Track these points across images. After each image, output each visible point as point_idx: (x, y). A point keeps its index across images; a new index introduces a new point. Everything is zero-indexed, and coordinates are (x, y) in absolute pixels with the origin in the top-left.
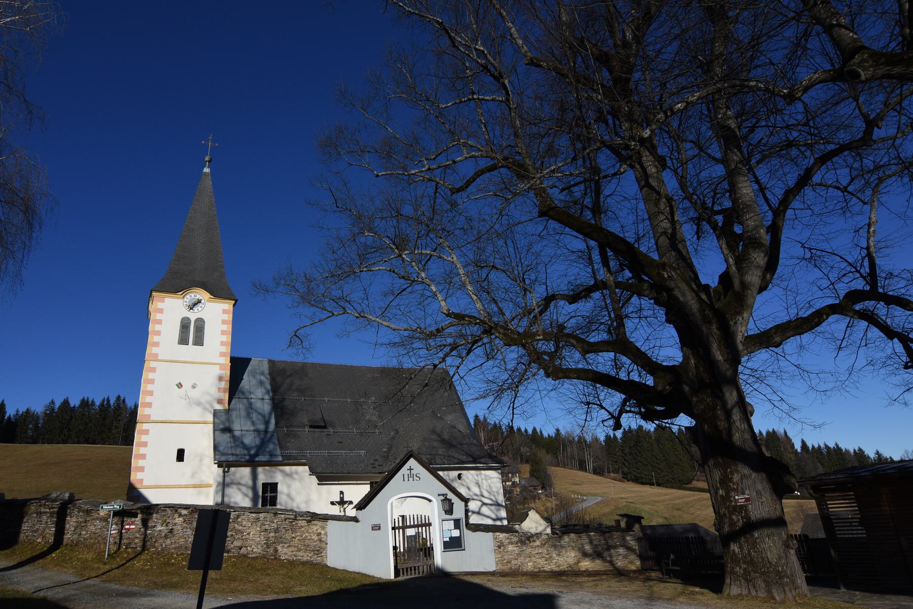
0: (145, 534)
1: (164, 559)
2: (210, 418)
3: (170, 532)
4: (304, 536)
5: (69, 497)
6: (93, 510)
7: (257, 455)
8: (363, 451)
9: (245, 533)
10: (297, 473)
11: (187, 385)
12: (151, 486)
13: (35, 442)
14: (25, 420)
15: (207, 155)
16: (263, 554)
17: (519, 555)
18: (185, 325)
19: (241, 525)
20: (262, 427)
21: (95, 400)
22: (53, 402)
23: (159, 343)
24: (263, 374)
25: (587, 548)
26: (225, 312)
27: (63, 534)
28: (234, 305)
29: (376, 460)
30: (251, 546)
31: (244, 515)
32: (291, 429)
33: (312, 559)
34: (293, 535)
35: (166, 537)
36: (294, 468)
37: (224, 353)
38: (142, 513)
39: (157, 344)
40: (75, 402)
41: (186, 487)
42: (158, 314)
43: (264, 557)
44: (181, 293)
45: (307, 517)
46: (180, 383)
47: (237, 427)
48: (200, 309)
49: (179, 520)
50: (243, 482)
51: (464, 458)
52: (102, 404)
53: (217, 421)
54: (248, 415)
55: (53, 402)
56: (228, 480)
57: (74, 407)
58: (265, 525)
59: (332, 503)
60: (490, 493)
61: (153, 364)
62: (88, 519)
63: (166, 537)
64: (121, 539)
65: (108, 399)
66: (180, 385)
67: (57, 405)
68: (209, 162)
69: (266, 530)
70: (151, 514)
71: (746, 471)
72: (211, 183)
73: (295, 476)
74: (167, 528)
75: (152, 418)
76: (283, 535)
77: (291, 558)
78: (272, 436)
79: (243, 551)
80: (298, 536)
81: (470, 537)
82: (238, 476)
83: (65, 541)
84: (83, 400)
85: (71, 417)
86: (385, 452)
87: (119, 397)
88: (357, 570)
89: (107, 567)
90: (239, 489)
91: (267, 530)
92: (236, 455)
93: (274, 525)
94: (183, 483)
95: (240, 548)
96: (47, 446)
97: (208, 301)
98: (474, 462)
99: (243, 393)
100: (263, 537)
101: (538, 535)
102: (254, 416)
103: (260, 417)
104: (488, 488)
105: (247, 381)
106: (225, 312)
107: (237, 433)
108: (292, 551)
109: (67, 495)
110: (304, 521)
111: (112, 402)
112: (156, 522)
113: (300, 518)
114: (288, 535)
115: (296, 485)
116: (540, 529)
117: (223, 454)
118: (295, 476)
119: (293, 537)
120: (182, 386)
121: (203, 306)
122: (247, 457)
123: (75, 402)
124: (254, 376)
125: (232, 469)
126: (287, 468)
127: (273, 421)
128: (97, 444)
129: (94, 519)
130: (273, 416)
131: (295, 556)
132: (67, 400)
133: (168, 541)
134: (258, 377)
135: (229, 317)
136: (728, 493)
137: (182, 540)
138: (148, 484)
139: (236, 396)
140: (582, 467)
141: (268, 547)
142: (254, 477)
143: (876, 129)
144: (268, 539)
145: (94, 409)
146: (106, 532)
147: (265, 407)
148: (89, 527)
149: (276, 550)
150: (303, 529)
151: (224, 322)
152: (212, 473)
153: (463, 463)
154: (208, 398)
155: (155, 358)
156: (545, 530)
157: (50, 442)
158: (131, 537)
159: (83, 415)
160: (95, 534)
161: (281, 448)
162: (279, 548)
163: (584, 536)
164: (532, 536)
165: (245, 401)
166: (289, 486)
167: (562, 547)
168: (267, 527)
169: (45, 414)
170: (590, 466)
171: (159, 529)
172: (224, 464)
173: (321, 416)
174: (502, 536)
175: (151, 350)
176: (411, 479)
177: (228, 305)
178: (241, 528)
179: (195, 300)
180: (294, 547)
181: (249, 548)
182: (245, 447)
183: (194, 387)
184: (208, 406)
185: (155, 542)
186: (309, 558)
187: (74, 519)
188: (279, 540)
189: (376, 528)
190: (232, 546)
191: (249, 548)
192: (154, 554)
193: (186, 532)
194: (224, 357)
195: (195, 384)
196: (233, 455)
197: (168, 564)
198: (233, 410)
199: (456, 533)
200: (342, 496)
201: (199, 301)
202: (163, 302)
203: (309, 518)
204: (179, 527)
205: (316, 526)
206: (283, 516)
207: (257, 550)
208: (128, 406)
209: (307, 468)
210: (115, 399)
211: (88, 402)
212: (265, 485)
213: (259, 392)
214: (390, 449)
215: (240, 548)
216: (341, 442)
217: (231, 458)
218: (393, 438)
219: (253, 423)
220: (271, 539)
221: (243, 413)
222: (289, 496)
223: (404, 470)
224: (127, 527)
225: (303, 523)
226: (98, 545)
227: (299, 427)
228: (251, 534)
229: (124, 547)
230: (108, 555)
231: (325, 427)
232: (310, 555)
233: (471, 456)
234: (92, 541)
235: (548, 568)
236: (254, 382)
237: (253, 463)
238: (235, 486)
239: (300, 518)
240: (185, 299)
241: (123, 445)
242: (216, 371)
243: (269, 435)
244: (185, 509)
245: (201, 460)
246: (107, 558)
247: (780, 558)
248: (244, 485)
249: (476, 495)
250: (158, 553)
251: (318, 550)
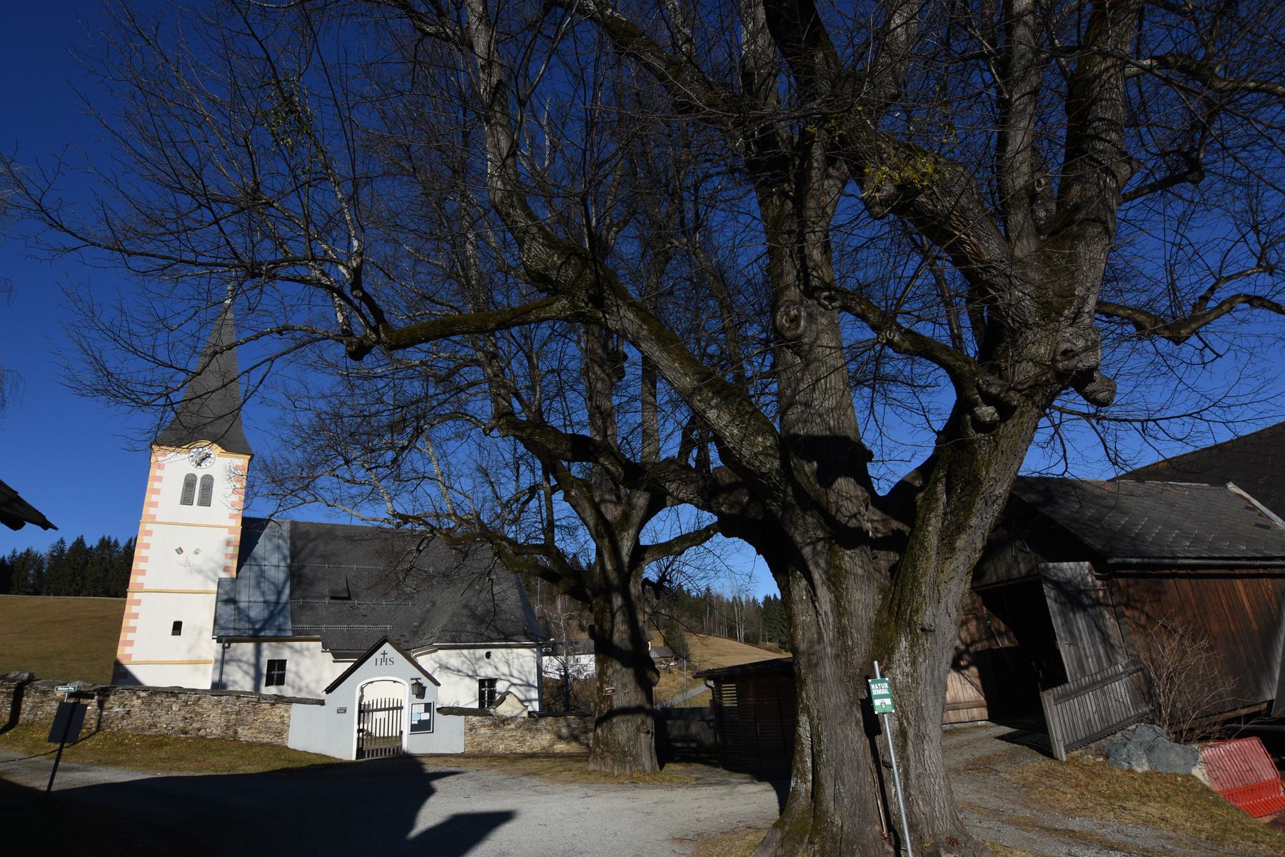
0: (100, 715)
2: (214, 588)
7: (261, 629)
10: (308, 649)
13: (37, 593)
14: (24, 563)
17: (491, 737)
18: (189, 483)
20: (272, 598)
22: (62, 542)
24: (281, 537)
25: (564, 731)
27: (19, 714)
32: (309, 600)
35: (123, 718)
36: (305, 644)
38: (98, 694)
39: (155, 504)
40: (92, 542)
47: (244, 598)
48: (208, 464)
49: (137, 702)
50: (244, 659)
51: (494, 635)
53: (220, 591)
54: (258, 585)
55: (62, 542)
56: (227, 657)
57: (91, 548)
60: (520, 672)
61: (148, 527)
63: (123, 718)
67: (68, 545)
69: (227, 713)
70: (108, 696)
71: (618, 666)
73: (306, 653)
75: (146, 587)
78: (284, 608)
79: (202, 732)
81: (440, 720)
82: (239, 652)
83: (20, 721)
84: (103, 539)
85: (87, 561)
86: (415, 627)
88: (318, 751)
90: (240, 667)
92: (239, 630)
93: (237, 708)
94: (178, 659)
96: (52, 598)
97: (219, 456)
98: (506, 639)
99: (255, 559)
101: (513, 719)
102: (265, 586)
103: (272, 587)
104: (519, 668)
105: (263, 546)
107: (242, 605)
109: (26, 675)
114: (250, 718)
115: (306, 663)
116: (516, 712)
117: (223, 628)
118: (306, 653)
122: (251, 632)
123: (92, 542)
124: (270, 540)
125: (233, 645)
126: (297, 644)
127: (287, 591)
130: (288, 585)
132: (82, 539)
133: (125, 722)
134: (276, 540)
136: (601, 685)
139: (248, 562)
140: (732, 635)
141: (228, 728)
142: (258, 653)
144: (228, 721)
147: (279, 575)
149: (236, 732)
152: (211, 649)
153: (492, 640)
154: (213, 565)
155: (152, 519)
156: (521, 713)
157: (57, 593)
159: (103, 559)
161: (293, 622)
162: (240, 730)
163: (561, 720)
164: (507, 719)
165: (256, 568)
166: (297, 664)
167: (538, 730)
168: (228, 709)
169: (52, 556)
170: (741, 633)
173: (345, 586)
174: (474, 719)
175: (148, 511)
176: (384, 663)
177: (241, 461)
179: (203, 455)
182: (250, 620)
183: (196, 553)
184: (211, 574)
187: (30, 700)
188: (240, 722)
189: (342, 711)
196: (235, 629)
197: (121, 744)
198: (241, 578)
199: (426, 716)
201: (208, 456)
204: (137, 709)
205: (280, 709)
207: (217, 732)
209: (320, 643)
211: (109, 542)
212: (271, 663)
213: (275, 558)
214: (421, 623)
215: (199, 730)
217: (232, 633)
218: (428, 611)
219: (263, 594)
221: (253, 582)
222: (297, 674)
223: (378, 655)
225: (267, 706)
227: (316, 598)
231: (349, 598)
233: (503, 633)
235: (519, 750)
236: (269, 546)
237: (256, 638)
238: (234, 663)
242: (224, 535)
245: (200, 634)
247: (629, 739)
248: (247, 663)
249: (504, 675)
250: (113, 734)
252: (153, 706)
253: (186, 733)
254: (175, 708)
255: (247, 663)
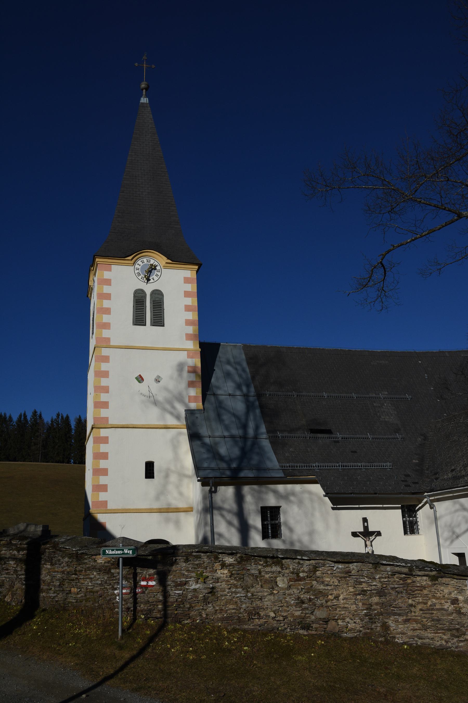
1: (211, 639)
3: (210, 593)
4: (429, 603)
5: (43, 531)
6: (86, 554)
8: (388, 464)
9: (330, 597)
10: (293, 494)
11: (149, 378)
12: (129, 509)
15: (143, 81)
16: (366, 634)
19: (323, 582)
20: (236, 432)
21: (12, 416)
26: (187, 280)
28: (197, 272)
29: (408, 476)
30: (343, 619)
31: (324, 565)
33: (450, 644)
34: (410, 601)
36: (289, 486)
41: (150, 511)
43: (367, 637)
44: (130, 258)
45: (431, 571)
46: (140, 375)
48: (156, 278)
49: (223, 573)
52: (19, 420)
58: (361, 583)
59: (355, 534)
62: (79, 568)
63: (205, 600)
64: (135, 602)
65: (25, 414)
66: (140, 379)
68: (147, 89)
69: (363, 592)
72: (151, 116)
73: (292, 498)
74: (206, 586)
75: (111, 422)
76: (395, 600)
77: (411, 641)
80: (419, 603)
87: (35, 412)
89: (127, 655)
91: (365, 591)
95: (326, 621)
97: (165, 267)
100: (360, 604)
102: (226, 417)
106: (187, 280)
108: (414, 630)
110: (425, 578)
111: (29, 418)
112: (187, 577)
113: (420, 573)
118: (292, 498)
119: (411, 605)
121: (159, 274)
122: (228, 473)
126: (281, 488)
128: (17, 461)
129: (89, 569)
131: (420, 638)
133: (210, 608)
135: (192, 287)
137: (231, 607)
138: (114, 508)
141: (372, 620)
142: (239, 498)
144: (369, 607)
145: (12, 425)
146: (110, 591)
148: (82, 581)
149: (385, 627)
150: (425, 592)
151: (187, 294)
158: (151, 600)
160: (93, 592)
162: (391, 623)
168: (364, 586)
171: (193, 587)
172: (211, 482)
178: (322, 587)
180: (416, 621)
181: (340, 622)
185: (189, 608)
186: (444, 643)
190: (313, 617)
191: (340, 622)
192: (191, 629)
193: (236, 593)
195: (159, 377)
200: (366, 524)
202: (110, 270)
203: (434, 573)
206: (389, 568)
208: (45, 421)
210: (31, 414)
216: (355, 452)
219: (227, 428)
220: (374, 607)
224: (144, 583)
225: (425, 581)
226: (100, 611)
228: (341, 597)
229: (143, 617)
230: (123, 631)
232: (445, 637)
234: (89, 604)
239: (420, 573)
240: (137, 266)
241: (43, 462)
243: (249, 443)
244: (229, 554)
246: (122, 637)
248: (229, 511)
251: (458, 630)
252: (249, 580)
253: (307, 627)
254: (282, 583)
255: (229, 511)
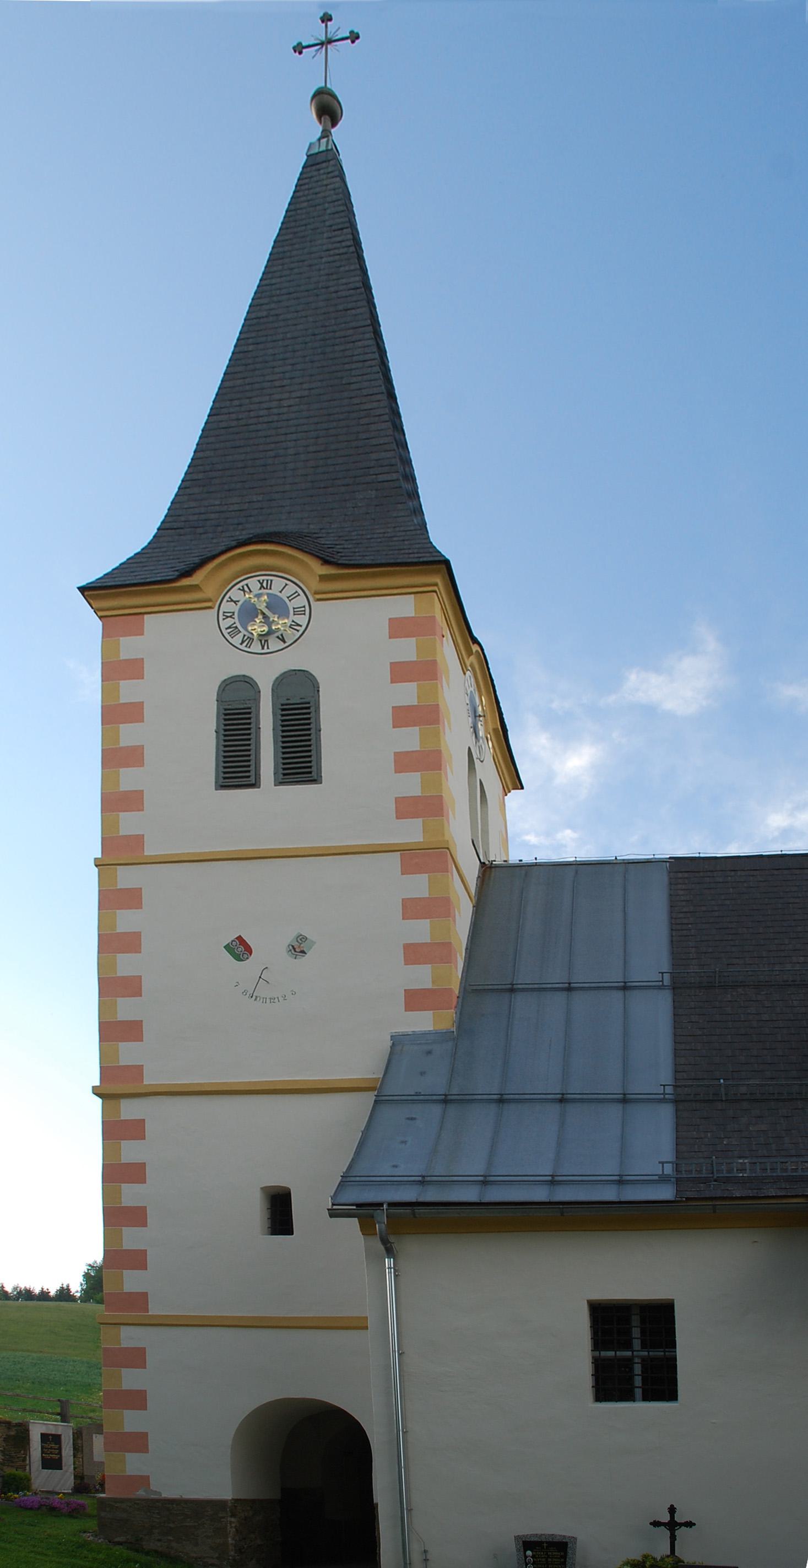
23: (141, 793)
37: (415, 799)
42: (416, 791)
75: (150, 1080)
120: (249, 950)
143: (50, 1294)
183: (298, 948)
194: (414, 816)
195: (302, 939)
